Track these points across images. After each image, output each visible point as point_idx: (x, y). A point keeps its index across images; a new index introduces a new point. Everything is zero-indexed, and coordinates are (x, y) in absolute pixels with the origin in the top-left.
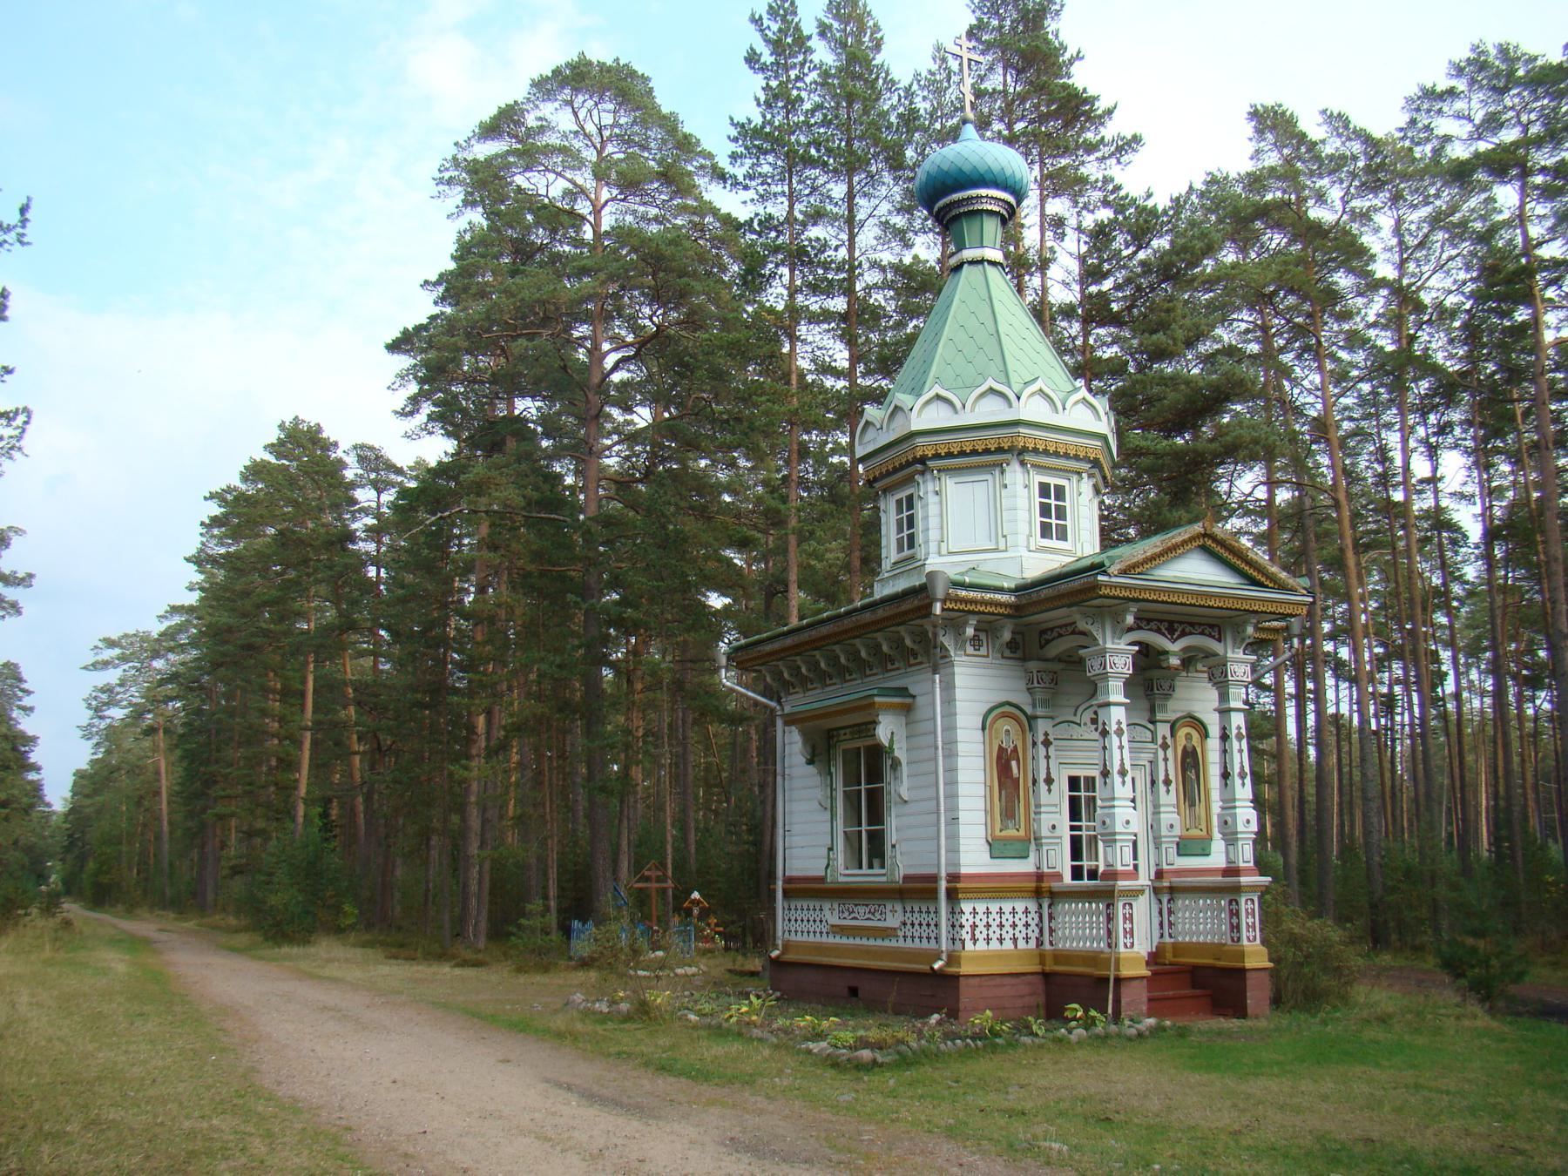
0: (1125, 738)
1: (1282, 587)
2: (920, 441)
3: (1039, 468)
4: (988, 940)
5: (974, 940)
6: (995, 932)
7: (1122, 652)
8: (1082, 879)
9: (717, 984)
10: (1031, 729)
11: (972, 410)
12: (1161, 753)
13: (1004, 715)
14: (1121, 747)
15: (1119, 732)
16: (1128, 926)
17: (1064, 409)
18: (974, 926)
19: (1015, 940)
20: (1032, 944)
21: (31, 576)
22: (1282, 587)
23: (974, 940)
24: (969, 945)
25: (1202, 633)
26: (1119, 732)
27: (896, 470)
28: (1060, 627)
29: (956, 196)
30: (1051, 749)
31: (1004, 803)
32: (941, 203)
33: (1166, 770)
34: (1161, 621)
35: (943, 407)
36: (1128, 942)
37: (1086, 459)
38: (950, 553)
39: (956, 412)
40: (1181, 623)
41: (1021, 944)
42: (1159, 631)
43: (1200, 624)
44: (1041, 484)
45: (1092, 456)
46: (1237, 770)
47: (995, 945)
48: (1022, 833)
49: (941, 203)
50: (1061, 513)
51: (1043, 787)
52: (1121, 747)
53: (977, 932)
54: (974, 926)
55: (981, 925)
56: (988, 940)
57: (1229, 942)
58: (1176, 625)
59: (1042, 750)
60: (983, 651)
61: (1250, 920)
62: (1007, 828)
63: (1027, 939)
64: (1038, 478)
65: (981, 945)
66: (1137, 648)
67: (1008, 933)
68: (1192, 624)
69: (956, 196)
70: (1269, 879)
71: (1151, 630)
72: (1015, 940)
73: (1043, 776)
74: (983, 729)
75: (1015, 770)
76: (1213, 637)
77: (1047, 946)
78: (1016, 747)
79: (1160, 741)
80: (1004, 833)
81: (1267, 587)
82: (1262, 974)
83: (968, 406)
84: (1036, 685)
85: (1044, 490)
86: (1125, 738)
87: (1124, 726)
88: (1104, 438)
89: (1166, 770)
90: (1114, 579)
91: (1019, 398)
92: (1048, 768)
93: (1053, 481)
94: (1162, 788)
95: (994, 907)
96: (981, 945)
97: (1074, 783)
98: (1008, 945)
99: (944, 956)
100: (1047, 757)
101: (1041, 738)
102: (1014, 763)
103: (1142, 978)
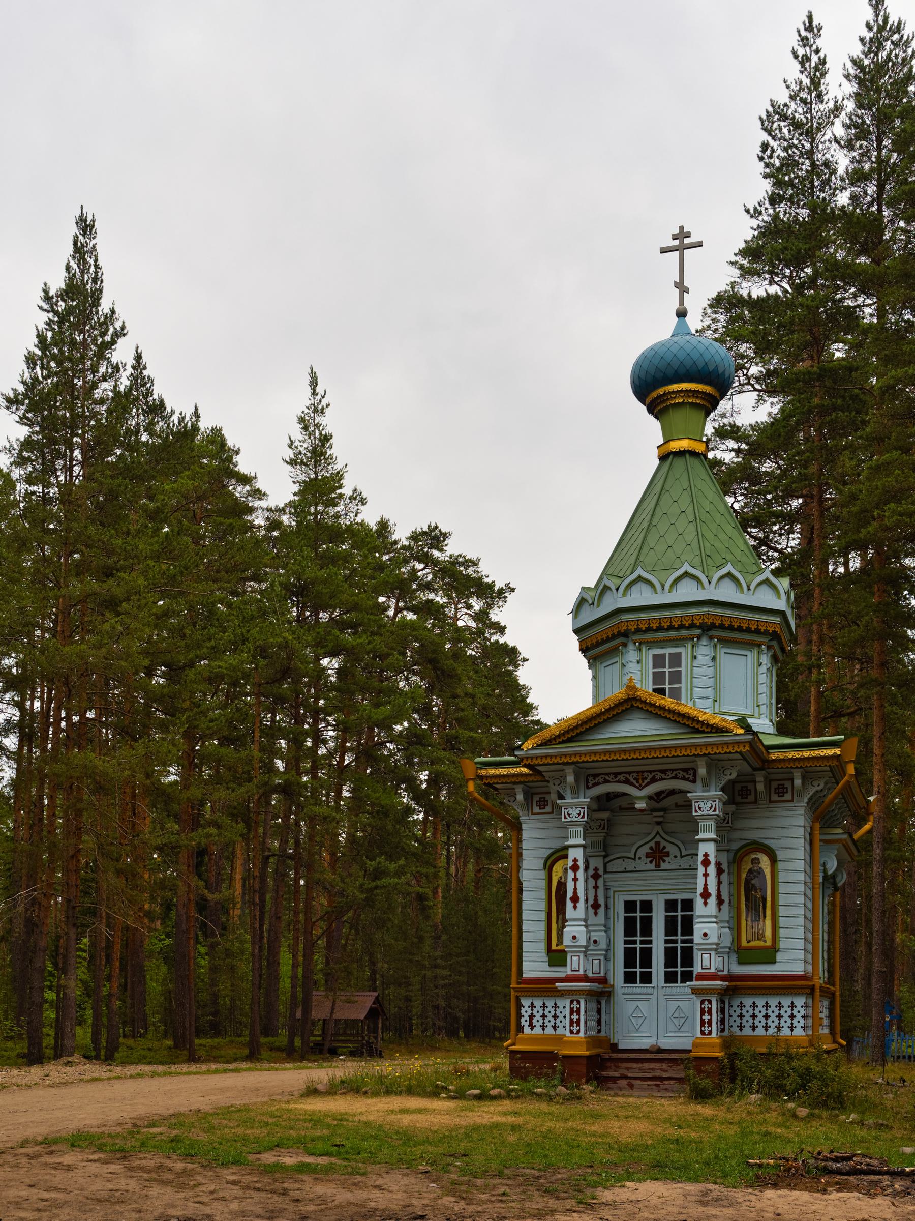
2: (625, 617)
3: (652, 644)
4: (543, 1027)
5: (532, 1027)
8: (670, 654)
9: (170, 1048)
17: (749, 589)
18: (532, 1017)
23: (532, 1027)
24: (527, 1030)
25: (675, 777)
27: (603, 642)
28: (607, 774)
29: (661, 391)
30: (600, 882)
32: (654, 395)
33: (575, 889)
34: (629, 773)
35: (693, 583)
37: (766, 633)
39: (703, 588)
40: (650, 772)
41: (786, 1032)
42: (627, 782)
43: (673, 770)
45: (771, 630)
49: (654, 395)
50: (676, 677)
53: (534, 1021)
54: (532, 1017)
55: (538, 1016)
56: (543, 1027)
61: (575, 1017)
64: (649, 654)
65: (538, 1030)
68: (664, 772)
69: (661, 391)
71: (619, 782)
74: (545, 868)
76: (687, 780)
80: (753, 944)
81: (703, 732)
83: (667, 586)
85: (658, 661)
88: (782, 613)
94: (569, 905)
96: (538, 1030)
97: (630, 906)
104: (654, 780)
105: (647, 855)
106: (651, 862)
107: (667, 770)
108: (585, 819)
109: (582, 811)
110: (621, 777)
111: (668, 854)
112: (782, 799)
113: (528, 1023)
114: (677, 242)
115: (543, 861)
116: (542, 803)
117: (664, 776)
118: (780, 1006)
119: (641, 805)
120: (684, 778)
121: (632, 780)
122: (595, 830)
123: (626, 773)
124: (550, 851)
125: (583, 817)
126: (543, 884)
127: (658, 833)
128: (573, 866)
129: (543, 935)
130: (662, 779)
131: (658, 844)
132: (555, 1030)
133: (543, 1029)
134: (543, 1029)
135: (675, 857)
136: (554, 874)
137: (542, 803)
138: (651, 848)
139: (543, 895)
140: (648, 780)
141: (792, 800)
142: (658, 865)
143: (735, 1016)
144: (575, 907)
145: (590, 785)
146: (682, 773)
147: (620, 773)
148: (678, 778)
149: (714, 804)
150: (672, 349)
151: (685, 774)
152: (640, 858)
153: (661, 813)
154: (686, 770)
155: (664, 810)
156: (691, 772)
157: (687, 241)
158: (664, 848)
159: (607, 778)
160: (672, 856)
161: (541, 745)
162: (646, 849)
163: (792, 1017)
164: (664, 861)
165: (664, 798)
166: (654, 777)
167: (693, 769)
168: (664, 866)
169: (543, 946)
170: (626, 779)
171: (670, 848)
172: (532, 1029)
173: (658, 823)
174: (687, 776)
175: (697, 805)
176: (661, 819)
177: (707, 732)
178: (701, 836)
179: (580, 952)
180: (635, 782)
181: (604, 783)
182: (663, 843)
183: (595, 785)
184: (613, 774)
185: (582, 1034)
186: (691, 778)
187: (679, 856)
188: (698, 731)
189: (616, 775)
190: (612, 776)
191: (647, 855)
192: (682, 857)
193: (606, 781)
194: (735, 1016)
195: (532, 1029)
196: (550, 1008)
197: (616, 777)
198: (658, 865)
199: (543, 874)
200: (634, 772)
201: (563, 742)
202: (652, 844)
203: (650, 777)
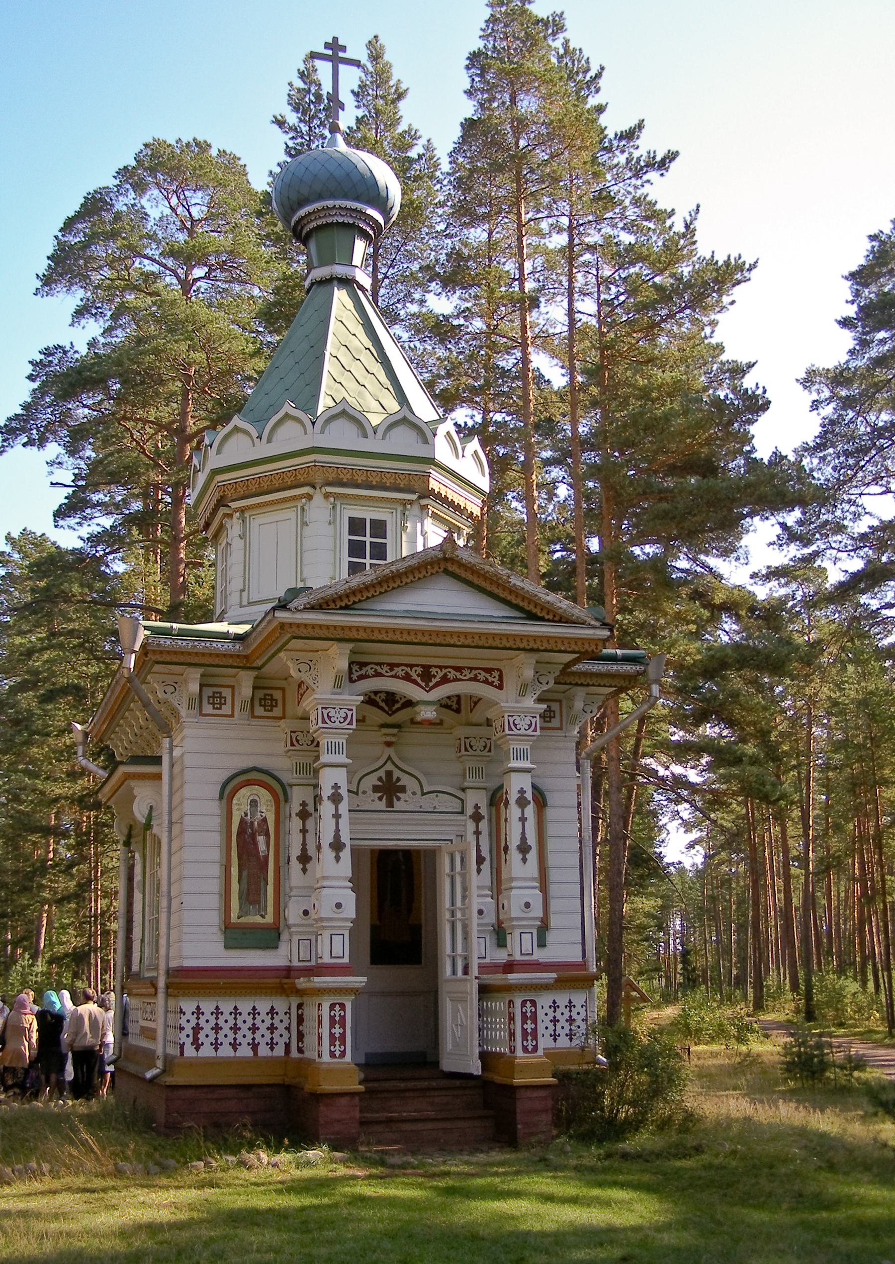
0: (344, 808)
1: (562, 619)
4: (216, 1045)
5: (197, 1045)
6: (226, 1036)
7: (526, 712)
10: (286, 800)
11: (269, 441)
12: (471, 826)
13: (249, 783)
14: (337, 816)
15: (336, 798)
16: (529, 1026)
18: (197, 1029)
19: (255, 1046)
20: (279, 1051)
21: (30, 362)
22: (562, 619)
23: (197, 1045)
24: (190, 1051)
25: (475, 679)
26: (336, 798)
29: (302, 212)
31: (245, 886)
34: (411, 666)
36: (530, 1045)
38: (250, 604)
40: (441, 667)
41: (263, 1051)
42: (407, 678)
43: (471, 669)
44: (352, 520)
46: (514, 841)
47: (226, 1051)
48: (269, 919)
51: (296, 866)
52: (337, 816)
53: (201, 1036)
54: (197, 1029)
55: (207, 1029)
56: (216, 1045)
57: (326, 1058)
58: (433, 671)
59: (296, 824)
60: (226, 709)
61: (337, 1030)
62: (247, 914)
63: (272, 1045)
66: (361, 698)
67: (245, 1037)
68: (458, 669)
69: (302, 212)
70: (365, 979)
71: (396, 676)
72: (255, 1046)
73: (296, 851)
74: (221, 797)
75: (262, 847)
76: (491, 684)
77: (294, 1054)
78: (265, 820)
79: (470, 811)
81: (542, 619)
82: (542, 1093)
84: (463, 752)
85: (356, 526)
86: (344, 808)
87: (343, 792)
89: (478, 846)
90: (298, 616)
91: (313, 423)
92: (304, 844)
93: (368, 514)
95: (227, 1006)
98: (245, 1051)
99: (160, 1063)
100: (304, 831)
101: (296, 808)
102: (261, 839)
103: (352, 1094)
104: (445, 680)
105: (376, 789)
106: (380, 799)
107: (464, 668)
108: (354, 726)
109: (349, 713)
110: (399, 671)
111: (403, 789)
112: (550, 725)
113: (191, 1039)
114: (330, 52)
115: (218, 788)
116: (217, 701)
117: (459, 676)
118: (217, 1012)
119: (428, 713)
120: (486, 682)
121: (415, 677)
122: (305, 747)
123: (406, 665)
124: (227, 774)
125: (350, 723)
126: (216, 822)
127: (389, 758)
128: (333, 794)
129: (215, 901)
130: (456, 680)
131: (389, 774)
132: (235, 1050)
133: (216, 1049)
134: (216, 1049)
135: (414, 793)
136: (234, 807)
137: (217, 701)
138: (380, 779)
139: (216, 838)
140: (437, 679)
141: (561, 729)
142: (390, 804)
143: (281, 1028)
144: (524, 860)
145: (355, 677)
146: (482, 675)
147: (398, 665)
148: (478, 681)
149: (533, 721)
150: (311, 168)
151: (487, 676)
152: (364, 792)
153: (395, 731)
154: (489, 671)
155: (398, 726)
156: (496, 674)
157: (341, 54)
158: (398, 779)
159: (379, 670)
160: (409, 792)
161: (313, 608)
162: (373, 780)
163: (235, 1029)
164: (399, 799)
165: (398, 709)
166: (445, 675)
167: (498, 670)
168: (398, 805)
169: (215, 918)
170: (407, 673)
171: (405, 780)
172: (197, 1049)
173: (389, 744)
174: (490, 679)
175: (511, 720)
176: (393, 739)
177: (548, 620)
178: (514, 764)
179: (531, 926)
180: (419, 680)
181: (374, 676)
182: (397, 773)
183: (361, 678)
184: (388, 664)
185: (348, 1058)
186: (497, 683)
187: (419, 793)
188: (532, 617)
189: (392, 666)
190: (386, 668)
191: (376, 789)
192: (423, 794)
193: (378, 674)
194: (281, 1028)
195: (197, 1049)
196: (226, 1016)
197: (391, 670)
198: (390, 804)
199: (215, 807)
200: (417, 666)
201: (347, 607)
202: (382, 773)
203: (441, 674)
